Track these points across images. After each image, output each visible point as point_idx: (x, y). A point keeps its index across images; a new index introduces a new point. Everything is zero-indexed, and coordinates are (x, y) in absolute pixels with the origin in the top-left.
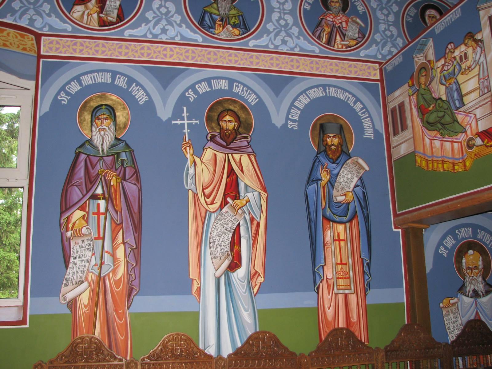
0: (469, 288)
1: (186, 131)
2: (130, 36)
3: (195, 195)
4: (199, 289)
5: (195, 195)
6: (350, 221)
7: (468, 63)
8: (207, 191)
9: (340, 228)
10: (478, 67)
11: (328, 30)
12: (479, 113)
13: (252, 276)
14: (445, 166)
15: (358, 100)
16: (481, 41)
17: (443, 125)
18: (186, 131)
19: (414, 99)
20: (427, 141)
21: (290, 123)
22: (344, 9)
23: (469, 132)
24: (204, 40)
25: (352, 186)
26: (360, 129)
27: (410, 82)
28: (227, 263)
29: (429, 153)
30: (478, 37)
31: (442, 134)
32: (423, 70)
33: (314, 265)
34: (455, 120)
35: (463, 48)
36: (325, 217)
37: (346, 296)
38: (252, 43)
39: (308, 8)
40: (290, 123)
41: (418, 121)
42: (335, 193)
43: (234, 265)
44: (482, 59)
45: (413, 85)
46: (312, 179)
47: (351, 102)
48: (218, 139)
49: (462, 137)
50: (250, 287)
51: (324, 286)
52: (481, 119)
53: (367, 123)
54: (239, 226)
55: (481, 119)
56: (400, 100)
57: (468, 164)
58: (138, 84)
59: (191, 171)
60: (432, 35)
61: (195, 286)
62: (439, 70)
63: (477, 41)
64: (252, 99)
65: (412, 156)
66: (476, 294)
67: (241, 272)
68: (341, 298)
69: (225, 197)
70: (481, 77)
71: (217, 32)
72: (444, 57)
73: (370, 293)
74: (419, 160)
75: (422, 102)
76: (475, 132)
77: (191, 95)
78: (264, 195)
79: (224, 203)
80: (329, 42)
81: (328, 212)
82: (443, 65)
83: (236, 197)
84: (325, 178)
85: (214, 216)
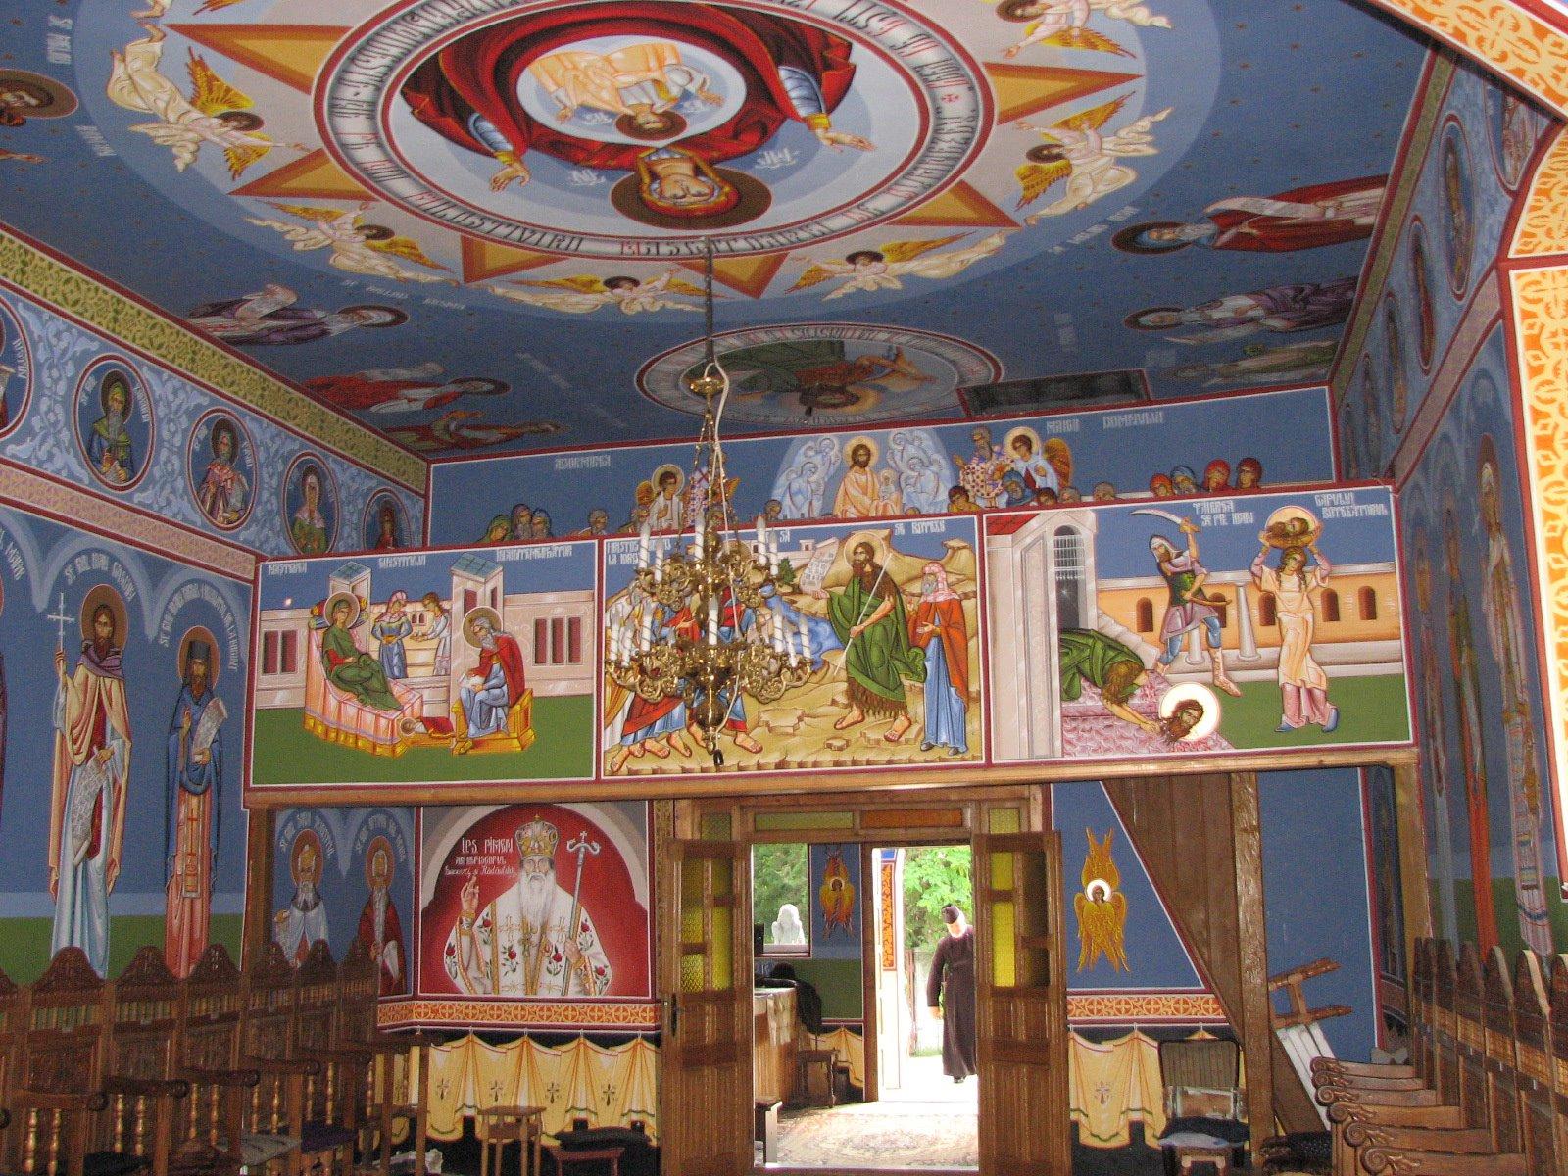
0: (301, 898)
1: (61, 633)
2: (13, 456)
3: (63, 737)
4: (57, 882)
5: (63, 737)
6: (204, 792)
7: (424, 629)
8: (76, 732)
9: (194, 800)
10: (436, 641)
11: (212, 489)
12: (427, 695)
13: (109, 865)
14: (360, 743)
15: (229, 610)
16: (447, 611)
17: (366, 689)
18: (61, 633)
19: (317, 637)
20: (333, 702)
21: (162, 637)
22: (232, 459)
23: (408, 712)
24: (91, 483)
25: (210, 740)
26: (226, 660)
27: (316, 611)
28: (86, 844)
29: (332, 717)
30: (446, 605)
31: (361, 701)
32: (343, 605)
33: (166, 855)
34: (387, 690)
35: (419, 607)
36: (182, 785)
37: (192, 901)
38: (139, 498)
39: (197, 448)
40: (162, 637)
41: (319, 669)
42: (194, 749)
43: (92, 851)
44: (445, 633)
45: (320, 616)
46: (175, 728)
47: (222, 611)
48: (91, 651)
49: (394, 715)
50: (106, 884)
51: (173, 885)
52: (428, 702)
53: (233, 648)
54: (101, 790)
55: (428, 702)
56: (289, 626)
57: (399, 750)
58: (16, 545)
59: (61, 700)
60: (373, 565)
61: (54, 878)
62: (373, 617)
63: (443, 611)
64: (129, 591)
65: (297, 715)
66: (305, 908)
67: (98, 860)
68: (187, 902)
69: (91, 747)
70: (440, 653)
71: (104, 470)
72: (388, 602)
73: (217, 898)
74: (311, 723)
75: (333, 646)
76: (417, 714)
77: (71, 578)
78: (128, 745)
79: (90, 754)
80: (211, 512)
81: (185, 777)
82: (383, 615)
83: (101, 746)
84: (187, 726)
85: (79, 771)
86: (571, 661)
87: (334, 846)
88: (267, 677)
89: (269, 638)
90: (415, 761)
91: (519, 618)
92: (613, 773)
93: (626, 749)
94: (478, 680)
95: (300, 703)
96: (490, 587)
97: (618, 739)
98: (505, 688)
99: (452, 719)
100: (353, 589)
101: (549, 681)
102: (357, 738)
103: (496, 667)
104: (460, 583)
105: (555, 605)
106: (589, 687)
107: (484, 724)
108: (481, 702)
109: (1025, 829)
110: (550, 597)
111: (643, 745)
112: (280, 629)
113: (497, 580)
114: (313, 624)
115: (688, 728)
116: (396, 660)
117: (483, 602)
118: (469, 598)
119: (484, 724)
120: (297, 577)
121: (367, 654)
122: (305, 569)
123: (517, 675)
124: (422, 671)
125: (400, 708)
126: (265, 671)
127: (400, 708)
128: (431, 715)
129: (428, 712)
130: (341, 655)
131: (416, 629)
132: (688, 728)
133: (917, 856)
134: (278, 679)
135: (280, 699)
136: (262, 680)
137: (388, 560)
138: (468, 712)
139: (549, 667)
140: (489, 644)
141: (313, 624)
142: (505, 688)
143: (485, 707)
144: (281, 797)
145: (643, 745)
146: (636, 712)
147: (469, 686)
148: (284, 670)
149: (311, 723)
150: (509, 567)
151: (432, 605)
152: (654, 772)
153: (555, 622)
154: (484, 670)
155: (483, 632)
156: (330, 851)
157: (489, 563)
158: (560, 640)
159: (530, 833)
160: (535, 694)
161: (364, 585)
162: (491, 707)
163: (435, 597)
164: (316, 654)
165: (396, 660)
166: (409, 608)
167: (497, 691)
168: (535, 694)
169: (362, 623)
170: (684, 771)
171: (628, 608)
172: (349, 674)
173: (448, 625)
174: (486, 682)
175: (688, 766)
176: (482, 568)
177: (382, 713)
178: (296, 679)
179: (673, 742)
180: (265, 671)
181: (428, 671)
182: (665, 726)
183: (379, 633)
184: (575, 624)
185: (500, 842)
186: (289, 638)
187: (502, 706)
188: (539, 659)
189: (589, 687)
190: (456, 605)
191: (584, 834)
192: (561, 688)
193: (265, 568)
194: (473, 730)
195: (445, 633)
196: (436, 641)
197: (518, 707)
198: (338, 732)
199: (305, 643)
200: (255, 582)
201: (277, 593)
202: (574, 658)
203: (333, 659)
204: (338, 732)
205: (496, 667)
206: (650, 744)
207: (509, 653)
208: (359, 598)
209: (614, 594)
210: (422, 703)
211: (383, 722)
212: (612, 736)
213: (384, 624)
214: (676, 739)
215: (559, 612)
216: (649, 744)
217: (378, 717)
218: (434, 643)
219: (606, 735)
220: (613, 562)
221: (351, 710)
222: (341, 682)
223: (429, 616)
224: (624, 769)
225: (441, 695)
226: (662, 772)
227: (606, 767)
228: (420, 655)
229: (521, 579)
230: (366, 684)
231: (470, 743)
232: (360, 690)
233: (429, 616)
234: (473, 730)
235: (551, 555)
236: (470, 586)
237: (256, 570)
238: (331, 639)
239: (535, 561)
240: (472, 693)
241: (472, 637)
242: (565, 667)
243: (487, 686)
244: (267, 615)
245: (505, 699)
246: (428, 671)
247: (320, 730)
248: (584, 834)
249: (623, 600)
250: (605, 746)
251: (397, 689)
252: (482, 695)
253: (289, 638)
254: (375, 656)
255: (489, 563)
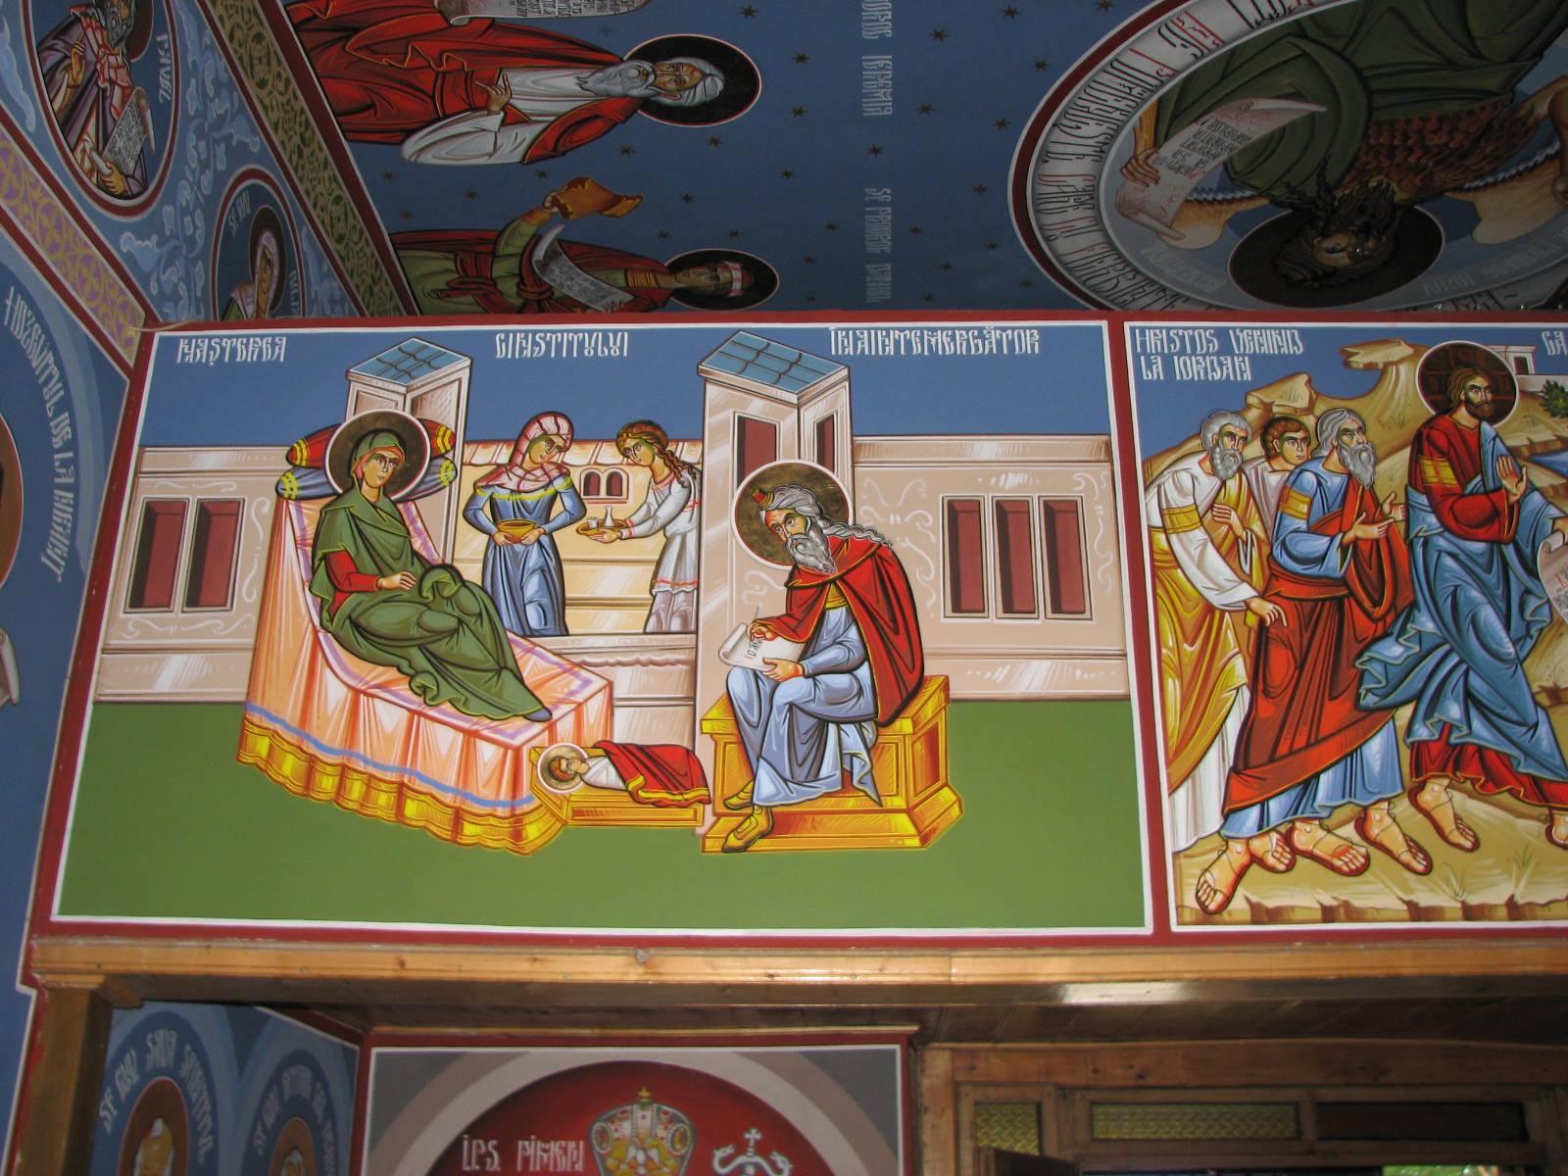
7: (620, 512)
10: (659, 540)
12: (625, 682)
14: (411, 808)
17: (439, 663)
20: (334, 692)
23: (565, 727)
27: (303, 453)
29: (329, 729)
30: (687, 453)
34: (504, 665)
35: (609, 454)
41: (298, 601)
44: (683, 523)
49: (523, 733)
52: (631, 702)
55: (631, 702)
56: (224, 489)
57: (532, 831)
62: (470, 475)
63: (675, 465)
65: (225, 722)
70: (667, 572)
74: (262, 746)
75: (344, 540)
76: (594, 733)
82: (499, 469)
86: (1057, 608)
87: (214, 1132)
88: (146, 618)
89: (160, 518)
90: (586, 867)
91: (901, 497)
92: (1207, 915)
93: (1237, 847)
94: (783, 649)
95: (236, 691)
96: (812, 415)
97: (1213, 820)
98: (864, 672)
99: (704, 752)
100: (415, 405)
101: (990, 657)
102: (402, 791)
103: (836, 616)
104: (724, 404)
105: (1003, 466)
106: (1118, 679)
107: (805, 763)
108: (792, 706)
109: (608, 739)
110: (987, 448)
111: (1287, 839)
112: (192, 493)
113: (835, 400)
114: (292, 485)
115: (1413, 794)
116: (533, 586)
117: (795, 449)
118: (754, 439)
119: (805, 763)
120: (259, 369)
121: (451, 569)
122: (281, 352)
123: (900, 642)
124: (611, 620)
125: (543, 715)
126: (138, 600)
127: (543, 715)
128: (623, 741)
129: (627, 729)
130: (367, 565)
131: (595, 511)
132: (1413, 794)
133: (1248, 106)
134: (174, 622)
135: (173, 679)
136: (122, 624)
137: (520, 340)
138: (753, 736)
139: (993, 624)
140: (813, 555)
141: (292, 485)
142: (864, 672)
143: (805, 723)
144: (149, 958)
145: (1287, 839)
146: (1259, 752)
147: (756, 664)
148: (193, 600)
149: (262, 746)
150: (862, 372)
151: (644, 452)
152: (1328, 914)
153: (1002, 509)
154: (799, 619)
155: (798, 525)
156: (206, 1142)
157: (809, 359)
158: (1021, 557)
159: (626, 1128)
160: (956, 692)
161: (446, 399)
162: (823, 723)
163: (655, 436)
164: (293, 564)
165: (533, 586)
166: (578, 457)
167: (841, 681)
168: (956, 692)
169: (438, 488)
170: (1416, 912)
171: (1208, 485)
172: (384, 619)
173: (694, 501)
174: (803, 657)
175: (1425, 899)
176: (793, 372)
177: (483, 726)
178: (228, 626)
179: (1374, 831)
180: (138, 600)
181: (634, 619)
182: (1347, 788)
183: (485, 517)
184: (1062, 517)
185: (555, 1147)
186: (218, 520)
187: (857, 721)
188: (964, 598)
189: (1118, 679)
190: (719, 456)
191: (753, 1135)
192: (1033, 679)
193: (170, 345)
194: (767, 785)
195: (683, 523)
196: (659, 540)
197: (905, 725)
198: (344, 771)
199: (263, 535)
200: (137, 375)
201: (215, 411)
202: (1067, 598)
203: (339, 576)
204: (344, 771)
205: (836, 616)
206: (1306, 836)
207: (877, 587)
208: (432, 427)
209: (1168, 447)
210: (611, 705)
211: (487, 753)
212: (1194, 808)
213: (502, 495)
214: (1380, 822)
215: (1012, 484)
216: (1306, 836)
217: (471, 735)
218: (652, 547)
219: (1177, 808)
220: (1157, 372)
221: (388, 716)
222: (364, 640)
223: (637, 479)
224: (1238, 903)
225: (673, 683)
226: (1352, 913)
227: (1183, 896)
228: (606, 577)
229: (894, 403)
230: (441, 648)
231: (760, 821)
232: (421, 662)
233: (637, 479)
234: (767, 785)
235: (988, 348)
236: (756, 409)
237: (146, 341)
238: (342, 521)
239: (934, 359)
240: (764, 682)
241: (762, 538)
242: (1041, 626)
243: (809, 664)
244: (156, 459)
245: (865, 704)
246: (634, 619)
247: (289, 766)
248: (753, 1135)
249: (1192, 463)
250: (1177, 837)
251: (533, 665)
252: (795, 689)
253: (218, 520)
254: (472, 573)
255: (809, 359)
